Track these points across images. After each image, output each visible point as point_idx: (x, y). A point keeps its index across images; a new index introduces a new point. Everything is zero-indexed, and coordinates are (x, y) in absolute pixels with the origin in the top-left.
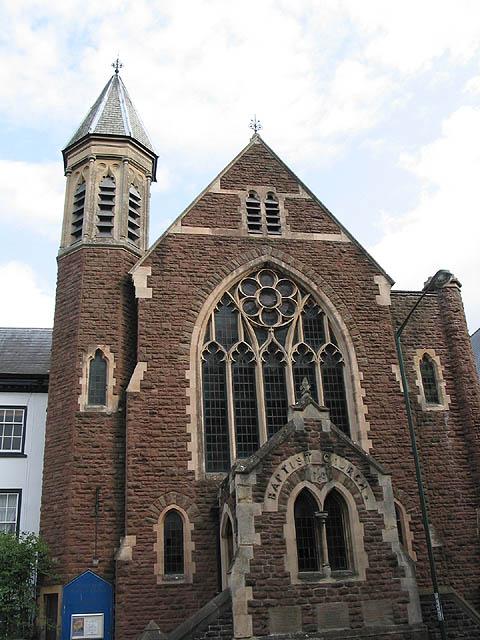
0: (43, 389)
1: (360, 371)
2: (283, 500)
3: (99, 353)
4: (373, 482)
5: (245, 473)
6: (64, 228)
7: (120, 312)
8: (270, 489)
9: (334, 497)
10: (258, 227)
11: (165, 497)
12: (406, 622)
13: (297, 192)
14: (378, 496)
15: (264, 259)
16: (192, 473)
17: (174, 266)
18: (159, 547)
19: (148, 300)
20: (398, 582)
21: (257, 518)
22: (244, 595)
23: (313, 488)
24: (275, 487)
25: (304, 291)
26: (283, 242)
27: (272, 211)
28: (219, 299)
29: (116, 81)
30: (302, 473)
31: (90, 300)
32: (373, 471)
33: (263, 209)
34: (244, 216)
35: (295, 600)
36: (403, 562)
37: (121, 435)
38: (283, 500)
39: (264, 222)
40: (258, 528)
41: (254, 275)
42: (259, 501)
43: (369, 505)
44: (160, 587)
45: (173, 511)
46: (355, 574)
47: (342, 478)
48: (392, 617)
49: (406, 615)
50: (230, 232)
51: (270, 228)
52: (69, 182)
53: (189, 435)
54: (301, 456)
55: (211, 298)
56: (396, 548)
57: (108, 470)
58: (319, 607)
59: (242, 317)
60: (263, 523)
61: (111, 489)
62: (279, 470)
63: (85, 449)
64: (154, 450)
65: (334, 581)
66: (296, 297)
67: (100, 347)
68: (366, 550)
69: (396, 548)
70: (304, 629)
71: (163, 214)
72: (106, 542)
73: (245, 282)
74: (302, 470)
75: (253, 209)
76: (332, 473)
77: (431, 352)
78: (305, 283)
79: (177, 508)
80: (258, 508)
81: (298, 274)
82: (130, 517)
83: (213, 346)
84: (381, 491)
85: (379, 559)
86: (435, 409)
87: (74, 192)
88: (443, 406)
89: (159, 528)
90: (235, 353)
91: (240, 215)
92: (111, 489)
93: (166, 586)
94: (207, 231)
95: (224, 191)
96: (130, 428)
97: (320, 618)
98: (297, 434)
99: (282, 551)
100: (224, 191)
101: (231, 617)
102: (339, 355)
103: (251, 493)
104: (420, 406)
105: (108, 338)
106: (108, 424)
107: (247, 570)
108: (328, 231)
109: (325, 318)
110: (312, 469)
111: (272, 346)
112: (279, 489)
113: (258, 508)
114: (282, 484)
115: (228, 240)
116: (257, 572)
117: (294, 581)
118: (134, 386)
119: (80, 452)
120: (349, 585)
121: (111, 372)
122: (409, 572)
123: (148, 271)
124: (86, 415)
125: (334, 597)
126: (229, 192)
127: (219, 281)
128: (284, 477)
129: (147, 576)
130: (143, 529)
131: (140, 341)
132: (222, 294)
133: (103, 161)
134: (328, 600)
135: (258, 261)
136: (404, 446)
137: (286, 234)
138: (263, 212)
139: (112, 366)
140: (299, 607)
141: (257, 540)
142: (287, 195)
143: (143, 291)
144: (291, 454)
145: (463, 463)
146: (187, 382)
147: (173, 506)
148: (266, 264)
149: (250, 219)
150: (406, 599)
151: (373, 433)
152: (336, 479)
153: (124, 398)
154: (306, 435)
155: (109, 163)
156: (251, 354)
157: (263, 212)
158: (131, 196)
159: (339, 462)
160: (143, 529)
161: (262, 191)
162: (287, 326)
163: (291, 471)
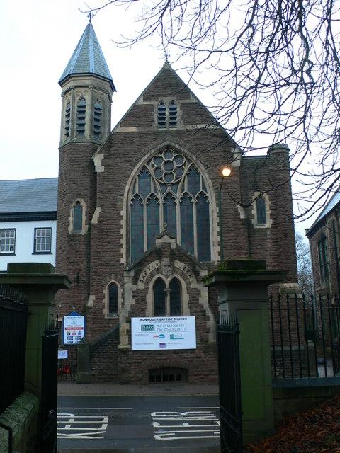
5: (129, 271)
6: (62, 131)
7: (88, 180)
8: (141, 278)
9: (175, 283)
10: (164, 124)
12: (207, 341)
15: (166, 143)
16: (123, 264)
18: (106, 301)
19: (102, 173)
24: (144, 277)
26: (178, 132)
27: (173, 112)
28: (141, 169)
29: (89, 29)
30: (158, 270)
33: (167, 112)
34: (156, 116)
37: (88, 245)
38: (147, 284)
40: (133, 297)
41: (160, 153)
42: (135, 284)
43: (193, 286)
44: (106, 319)
50: (148, 129)
51: (171, 124)
52: (63, 102)
54: (158, 261)
57: (83, 264)
59: (153, 179)
60: (135, 294)
66: (184, 165)
67: (78, 200)
71: (120, 107)
73: (155, 158)
74: (158, 269)
75: (162, 113)
76: (174, 270)
80: (134, 287)
81: (185, 151)
82: (93, 286)
83: (137, 196)
86: (263, 227)
88: (269, 223)
89: (106, 292)
90: (148, 199)
93: (109, 319)
95: (145, 103)
98: (157, 251)
100: (145, 103)
101: (119, 336)
103: (131, 279)
104: (253, 225)
106: (83, 239)
111: (169, 194)
113: (134, 287)
115: (145, 133)
118: (94, 221)
121: (84, 213)
123: (102, 156)
124: (73, 236)
126: (148, 103)
127: (132, 170)
128: (148, 272)
133: (79, 89)
137: (180, 126)
138: (167, 114)
139: (84, 210)
141: (133, 302)
142: (183, 101)
143: (99, 168)
145: (276, 258)
148: (168, 146)
155: (82, 90)
156: (157, 199)
157: (167, 114)
158: (96, 108)
159: (179, 265)
161: (167, 100)
162: (179, 182)
163: (152, 269)
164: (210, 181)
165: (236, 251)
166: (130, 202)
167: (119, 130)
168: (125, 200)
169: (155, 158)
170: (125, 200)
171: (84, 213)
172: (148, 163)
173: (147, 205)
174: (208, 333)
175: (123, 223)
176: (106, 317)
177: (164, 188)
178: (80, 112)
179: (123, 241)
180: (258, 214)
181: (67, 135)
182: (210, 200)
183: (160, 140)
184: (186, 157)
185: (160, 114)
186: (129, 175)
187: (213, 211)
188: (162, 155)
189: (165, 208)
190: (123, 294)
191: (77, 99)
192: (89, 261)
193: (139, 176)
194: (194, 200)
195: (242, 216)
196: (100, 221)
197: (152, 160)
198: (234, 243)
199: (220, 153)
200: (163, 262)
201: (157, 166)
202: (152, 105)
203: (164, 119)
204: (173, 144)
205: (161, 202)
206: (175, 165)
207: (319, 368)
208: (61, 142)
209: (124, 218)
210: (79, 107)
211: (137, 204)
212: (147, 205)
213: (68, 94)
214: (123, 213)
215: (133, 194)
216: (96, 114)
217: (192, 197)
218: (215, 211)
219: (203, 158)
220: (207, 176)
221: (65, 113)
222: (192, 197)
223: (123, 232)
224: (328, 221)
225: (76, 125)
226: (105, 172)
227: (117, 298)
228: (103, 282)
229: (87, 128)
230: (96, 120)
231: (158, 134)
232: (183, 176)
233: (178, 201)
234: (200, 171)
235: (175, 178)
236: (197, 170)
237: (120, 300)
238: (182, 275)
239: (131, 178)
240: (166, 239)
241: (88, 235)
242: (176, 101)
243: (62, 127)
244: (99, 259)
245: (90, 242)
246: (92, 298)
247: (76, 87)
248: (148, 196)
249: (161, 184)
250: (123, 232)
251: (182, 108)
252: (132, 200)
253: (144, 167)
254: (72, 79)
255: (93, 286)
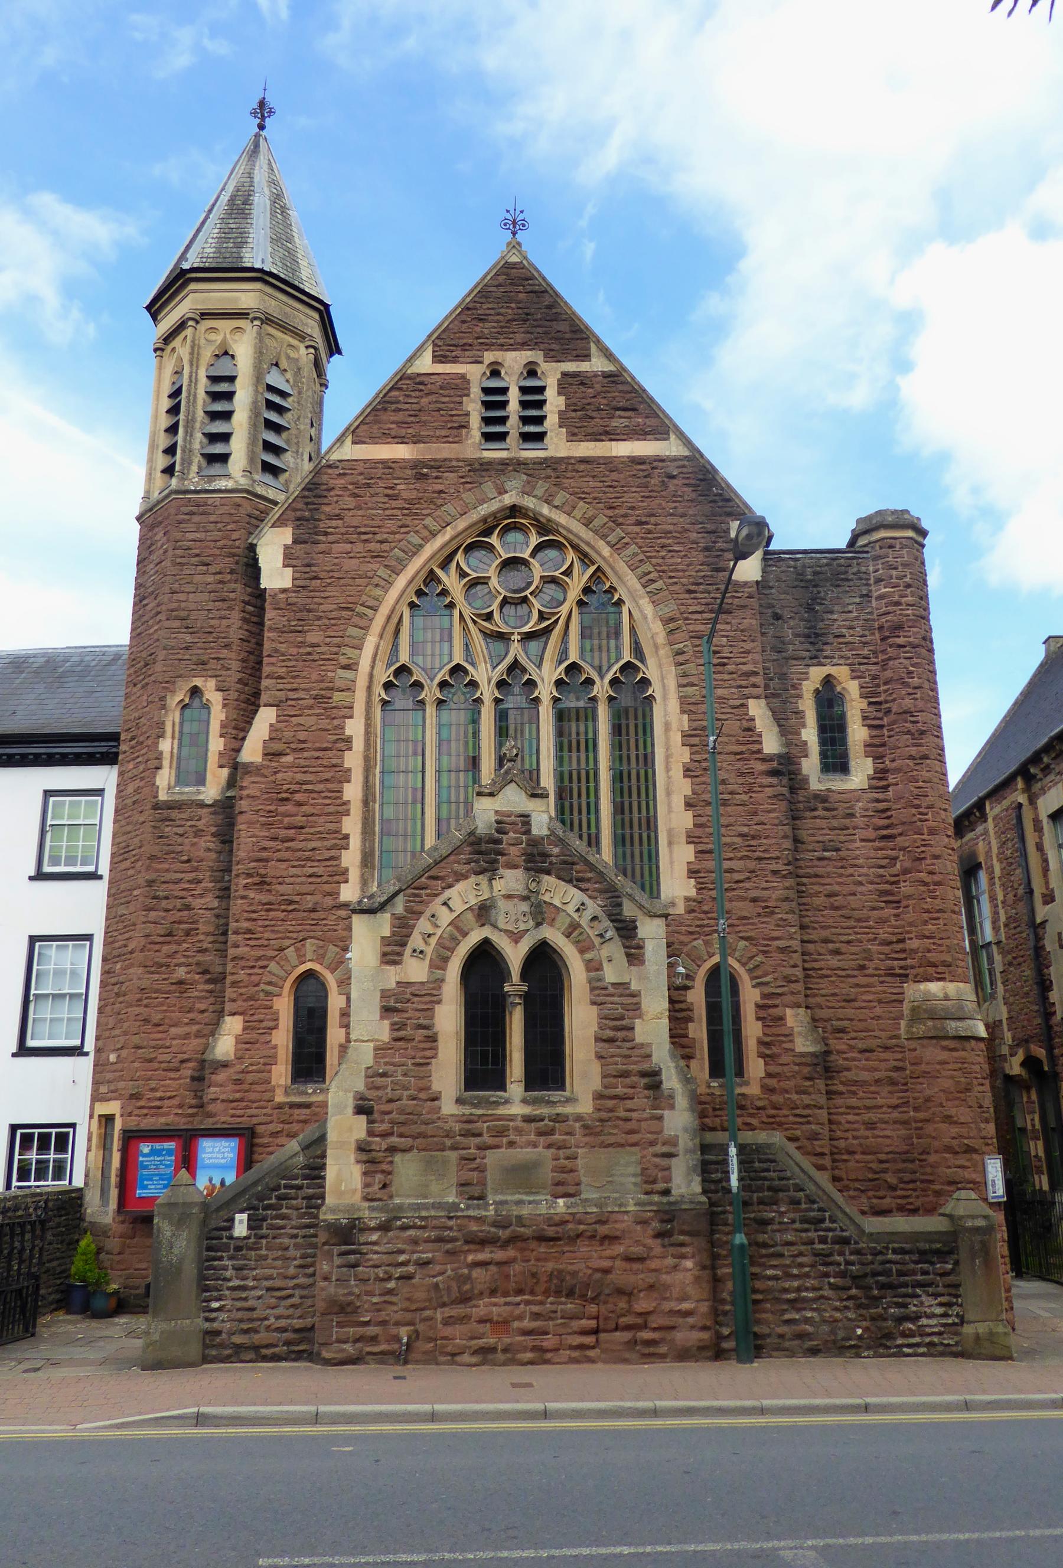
0: (109, 759)
1: (683, 712)
2: (441, 962)
3: (195, 691)
4: (627, 930)
6: (151, 461)
7: (236, 615)
8: (416, 941)
10: (502, 437)
11: (297, 950)
12: (666, 1192)
13: (587, 357)
14: (634, 955)
15: (508, 499)
17: (334, 523)
18: (283, 1038)
19: (284, 591)
20: (660, 1118)
21: (385, 994)
22: (350, 1130)
23: (502, 943)
25: (585, 558)
27: (532, 400)
28: (419, 583)
30: (484, 912)
31: (182, 597)
32: (629, 910)
33: (514, 397)
34: (474, 408)
35: (448, 1142)
36: (671, 1081)
37: (226, 837)
38: (441, 962)
39: (513, 426)
40: (387, 1010)
41: (488, 532)
44: (280, 1106)
45: (310, 974)
46: (747, 1083)
47: (563, 922)
48: (639, 1180)
49: (668, 1180)
52: (160, 368)
53: (346, 837)
54: (483, 879)
55: (401, 582)
56: (662, 1055)
58: (492, 1158)
61: (207, 934)
62: (436, 906)
63: (166, 866)
64: (284, 865)
65: (527, 1110)
66: (568, 572)
67: (198, 682)
68: (600, 1057)
69: (662, 1055)
70: (460, 1194)
72: (195, 1028)
76: (541, 913)
77: (841, 672)
78: (588, 544)
79: (317, 967)
80: (392, 977)
82: (234, 984)
84: (640, 947)
85: (625, 1074)
87: (167, 389)
89: (284, 1006)
90: (443, 685)
91: (468, 414)
92: (207, 934)
93: (293, 1106)
94: (402, 452)
95: (440, 368)
96: (241, 827)
97: (492, 1177)
99: (428, 1053)
100: (440, 368)
102: (645, 682)
104: (806, 780)
105: (212, 664)
106: (206, 821)
107: (360, 1085)
108: (642, 434)
109: (625, 610)
110: (502, 904)
111: (515, 666)
112: (433, 941)
114: (439, 932)
115: (439, 466)
116: (378, 1088)
117: (448, 1107)
118: (252, 751)
119: (157, 871)
120: (559, 1118)
121: (215, 727)
122: (682, 1101)
123: (286, 535)
124: (170, 806)
125: (524, 1139)
128: (445, 917)
129: (258, 1088)
130: (257, 1004)
131: (266, 670)
132: (423, 574)
134: (511, 1144)
135: (494, 506)
136: (760, 859)
139: (218, 715)
140: (453, 1156)
141: (384, 1032)
144: (461, 877)
146: (349, 740)
147: (309, 966)
148: (514, 510)
149: (487, 421)
150: (672, 1150)
151: (699, 832)
152: (552, 923)
153: (236, 770)
154: (499, 842)
155: (225, 325)
156: (473, 684)
158: (270, 388)
160: (257, 1004)
161: (514, 361)
162: (547, 631)
163: (459, 907)
164: (658, 627)
165: (752, 865)
166: (379, 691)
167: (349, 451)
168: (361, 683)
169: (470, 548)
170: (361, 683)
171: (215, 727)
172: (444, 565)
173: (440, 702)
174: (670, 1155)
175: (353, 760)
176: (280, 1098)
177: (499, 646)
178: (215, 396)
179: (352, 825)
180: (823, 742)
181: (169, 471)
182: (655, 689)
183: (489, 488)
184: (576, 548)
185: (488, 405)
186: (379, 600)
187: (667, 727)
188: (494, 540)
189: (502, 716)
190: (345, 1014)
191: (207, 355)
192: (225, 893)
193: (412, 605)
194: (601, 689)
195: (771, 745)
196: (270, 755)
197: (460, 556)
198: (742, 835)
199: (694, 536)
200: (498, 884)
201: (474, 575)
202: (463, 377)
203: (503, 420)
204: (529, 502)
205: (487, 692)
206: (537, 571)
207: (237, 1140)
208: (147, 497)
209: (358, 744)
210: (214, 379)
211: (402, 700)
212: (440, 702)
213: (177, 342)
214: (354, 728)
215: (389, 665)
216: (271, 405)
217: (596, 678)
218: (674, 725)
219: (633, 548)
220: (648, 609)
221: (166, 404)
222: (596, 678)
223: (353, 792)
224: (993, 810)
225: (199, 436)
226: (297, 588)
227: (322, 1030)
228: (273, 966)
229: (238, 448)
230: (270, 425)
231: (484, 468)
232: (564, 610)
233: (545, 691)
234: (622, 592)
235: (535, 615)
236: (612, 590)
237: (334, 1035)
238: (572, 930)
239: (384, 610)
240: (513, 799)
241: (226, 808)
242: (544, 367)
243: (152, 447)
244: (262, 884)
245: (231, 825)
246: (233, 1026)
247: (205, 315)
248: (442, 675)
249: (489, 635)
250: (353, 792)
251: (562, 389)
252: (388, 686)
253: (431, 578)
254: (193, 286)
255: (234, 984)
